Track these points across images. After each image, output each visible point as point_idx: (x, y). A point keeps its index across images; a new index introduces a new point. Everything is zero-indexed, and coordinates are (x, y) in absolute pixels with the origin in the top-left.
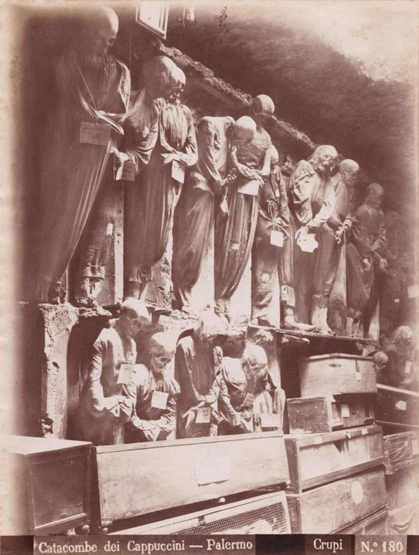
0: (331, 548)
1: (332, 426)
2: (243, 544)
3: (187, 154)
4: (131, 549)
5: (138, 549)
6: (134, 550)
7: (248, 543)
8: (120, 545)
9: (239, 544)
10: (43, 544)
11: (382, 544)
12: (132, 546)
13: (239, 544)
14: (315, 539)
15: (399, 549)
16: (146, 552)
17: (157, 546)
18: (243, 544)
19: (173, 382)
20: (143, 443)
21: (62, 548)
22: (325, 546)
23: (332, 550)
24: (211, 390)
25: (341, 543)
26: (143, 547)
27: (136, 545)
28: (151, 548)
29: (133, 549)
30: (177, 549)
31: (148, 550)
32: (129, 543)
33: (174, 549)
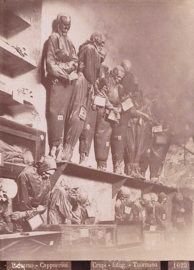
0: (101, 267)
1: (66, 191)
2: (29, 265)
3: (116, 205)
4: (42, 267)
5: (45, 266)
6: (43, 267)
7: (122, 264)
8: (106, 264)
9: (27, 265)
10: (42, 263)
11: (174, 264)
12: (42, 265)
13: (27, 265)
14: (41, 262)
15: (115, 266)
16: (49, 268)
17: (54, 265)
18: (29, 265)
19: (64, 161)
20: (22, 166)
21: (30, 265)
22: (98, 266)
23: (101, 268)
24: (52, 149)
25: (67, 264)
26: (47, 265)
27: (44, 265)
28: (51, 266)
29: (42, 266)
30: (101, 265)
31: (50, 267)
32: (41, 263)
33: (62, 267)
